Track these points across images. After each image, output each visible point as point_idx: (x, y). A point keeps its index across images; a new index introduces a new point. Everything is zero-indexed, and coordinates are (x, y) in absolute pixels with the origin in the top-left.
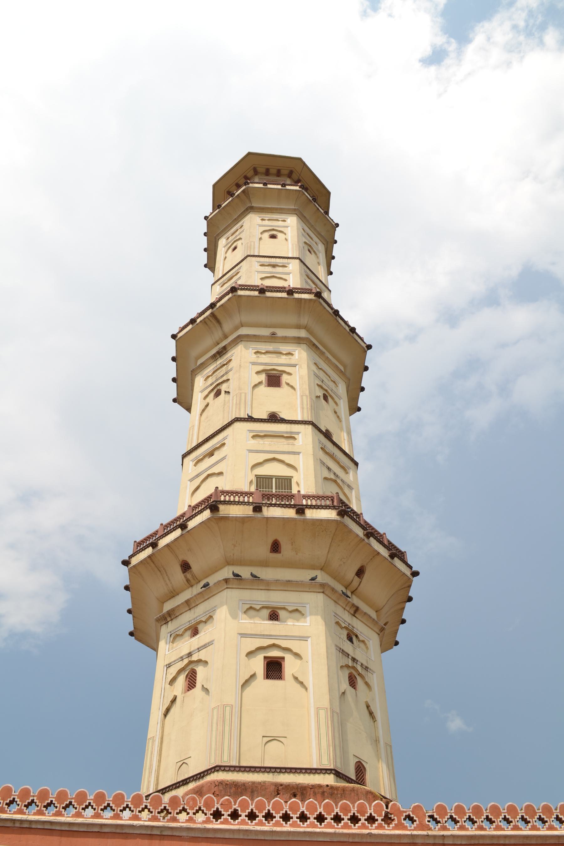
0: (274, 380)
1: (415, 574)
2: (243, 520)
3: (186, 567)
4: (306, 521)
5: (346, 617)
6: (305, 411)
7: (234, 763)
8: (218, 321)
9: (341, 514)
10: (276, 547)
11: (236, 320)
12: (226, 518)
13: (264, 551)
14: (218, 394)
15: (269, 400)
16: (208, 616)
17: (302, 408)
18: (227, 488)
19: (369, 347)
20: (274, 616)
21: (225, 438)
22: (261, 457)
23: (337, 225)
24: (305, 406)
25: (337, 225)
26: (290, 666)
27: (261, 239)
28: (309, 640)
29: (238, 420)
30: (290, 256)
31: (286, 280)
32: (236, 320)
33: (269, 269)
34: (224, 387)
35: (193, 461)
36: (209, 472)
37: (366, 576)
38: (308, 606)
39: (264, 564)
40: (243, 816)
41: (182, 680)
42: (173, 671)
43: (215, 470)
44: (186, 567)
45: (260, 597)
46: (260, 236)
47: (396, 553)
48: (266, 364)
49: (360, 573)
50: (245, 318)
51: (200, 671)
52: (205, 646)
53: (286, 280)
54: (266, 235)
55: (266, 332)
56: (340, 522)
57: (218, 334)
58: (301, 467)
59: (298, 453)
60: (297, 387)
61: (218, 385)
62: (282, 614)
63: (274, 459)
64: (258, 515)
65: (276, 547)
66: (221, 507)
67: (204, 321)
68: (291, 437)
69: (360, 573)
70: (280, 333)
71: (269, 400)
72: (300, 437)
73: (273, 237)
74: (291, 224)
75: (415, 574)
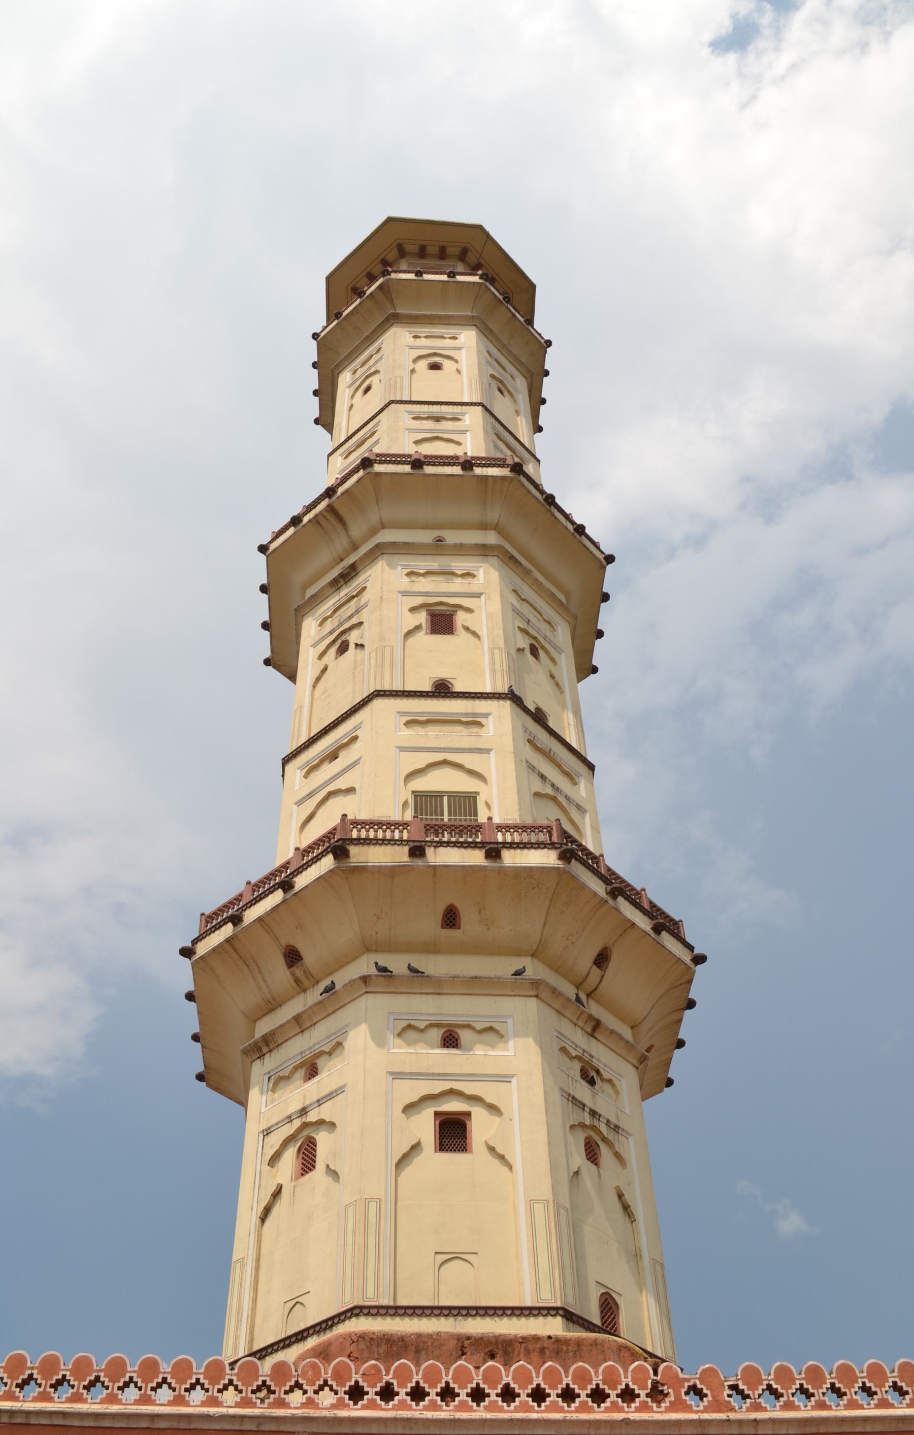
1: (700, 959)
2: (392, 872)
3: (293, 957)
4: (504, 872)
6: (499, 675)
7: (386, 1301)
8: (341, 520)
9: (566, 856)
10: (451, 918)
11: (373, 517)
12: (361, 870)
13: (429, 925)
14: (343, 648)
15: (433, 658)
16: (334, 1042)
17: (493, 671)
19: (610, 559)
20: (450, 1040)
21: (357, 728)
24: (498, 667)
25: (549, 343)
26: (481, 1128)
27: (413, 371)
28: (514, 1080)
30: (466, 400)
31: (459, 444)
32: (373, 517)
36: (331, 788)
38: (510, 1021)
39: (432, 948)
44: (293, 957)
45: (426, 1006)
46: (412, 366)
47: (665, 924)
49: (602, 960)
50: (388, 513)
51: (323, 1139)
52: (330, 1096)
53: (459, 444)
54: (423, 365)
55: (425, 537)
56: (564, 871)
58: (492, 774)
59: (488, 751)
60: (484, 633)
61: (343, 633)
62: (465, 1036)
63: (445, 763)
64: (419, 862)
65: (451, 918)
68: (474, 723)
69: (602, 960)
70: (452, 537)
71: (433, 658)
72: (490, 723)
73: (435, 367)
74: (467, 343)
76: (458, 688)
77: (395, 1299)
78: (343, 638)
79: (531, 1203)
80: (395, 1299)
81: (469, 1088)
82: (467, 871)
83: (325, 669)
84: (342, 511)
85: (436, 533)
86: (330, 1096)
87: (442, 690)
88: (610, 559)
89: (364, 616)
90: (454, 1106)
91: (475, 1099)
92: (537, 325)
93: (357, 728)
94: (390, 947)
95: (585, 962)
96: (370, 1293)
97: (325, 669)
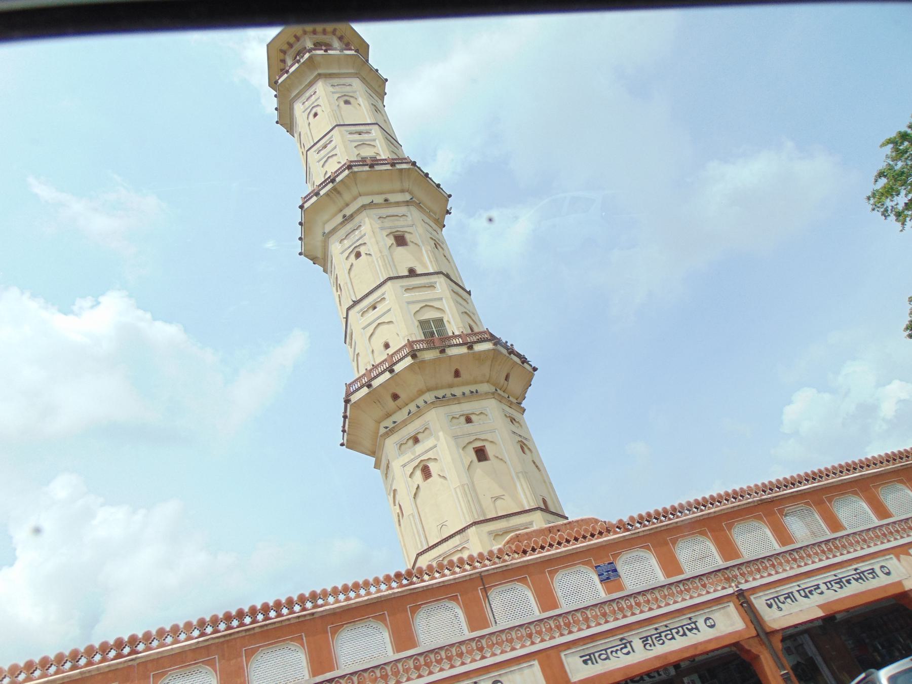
0: (401, 240)
1: (535, 369)
4: (474, 353)
5: (507, 409)
7: (482, 519)
8: (339, 193)
9: (495, 344)
10: (457, 374)
11: (355, 191)
12: (423, 362)
13: (449, 378)
14: (358, 255)
15: (404, 259)
18: (414, 339)
19: (450, 196)
20: (469, 420)
21: (383, 294)
22: (417, 307)
23: (386, 80)
25: (386, 80)
26: (490, 450)
29: (390, 279)
30: (369, 122)
32: (355, 191)
33: (357, 137)
34: (362, 250)
35: (358, 312)
36: (379, 321)
37: (510, 380)
39: (451, 386)
40: (530, 551)
41: (418, 474)
42: (409, 469)
43: (385, 319)
45: (457, 409)
47: (524, 360)
48: (390, 228)
49: (507, 378)
51: (432, 466)
52: (431, 449)
54: (342, 103)
55: (378, 199)
57: (340, 203)
58: (447, 309)
59: (441, 299)
62: (473, 417)
63: (426, 306)
64: (444, 355)
65: (457, 374)
66: (418, 354)
67: (327, 194)
68: (432, 286)
69: (507, 378)
70: (393, 198)
71: (404, 259)
72: (438, 285)
73: (316, 115)
75: (535, 369)
76: (419, 272)
77: (496, 512)
78: (357, 250)
79: (517, 473)
80: (496, 512)
81: (483, 437)
82: (461, 356)
83: (352, 265)
84: (339, 189)
85: (384, 196)
86: (431, 449)
87: (412, 273)
88: (450, 196)
89: (365, 239)
90: (478, 444)
91: (486, 440)
92: (371, 61)
93: (383, 294)
94: (436, 388)
95: (502, 380)
96: (468, 519)
97: (352, 265)
